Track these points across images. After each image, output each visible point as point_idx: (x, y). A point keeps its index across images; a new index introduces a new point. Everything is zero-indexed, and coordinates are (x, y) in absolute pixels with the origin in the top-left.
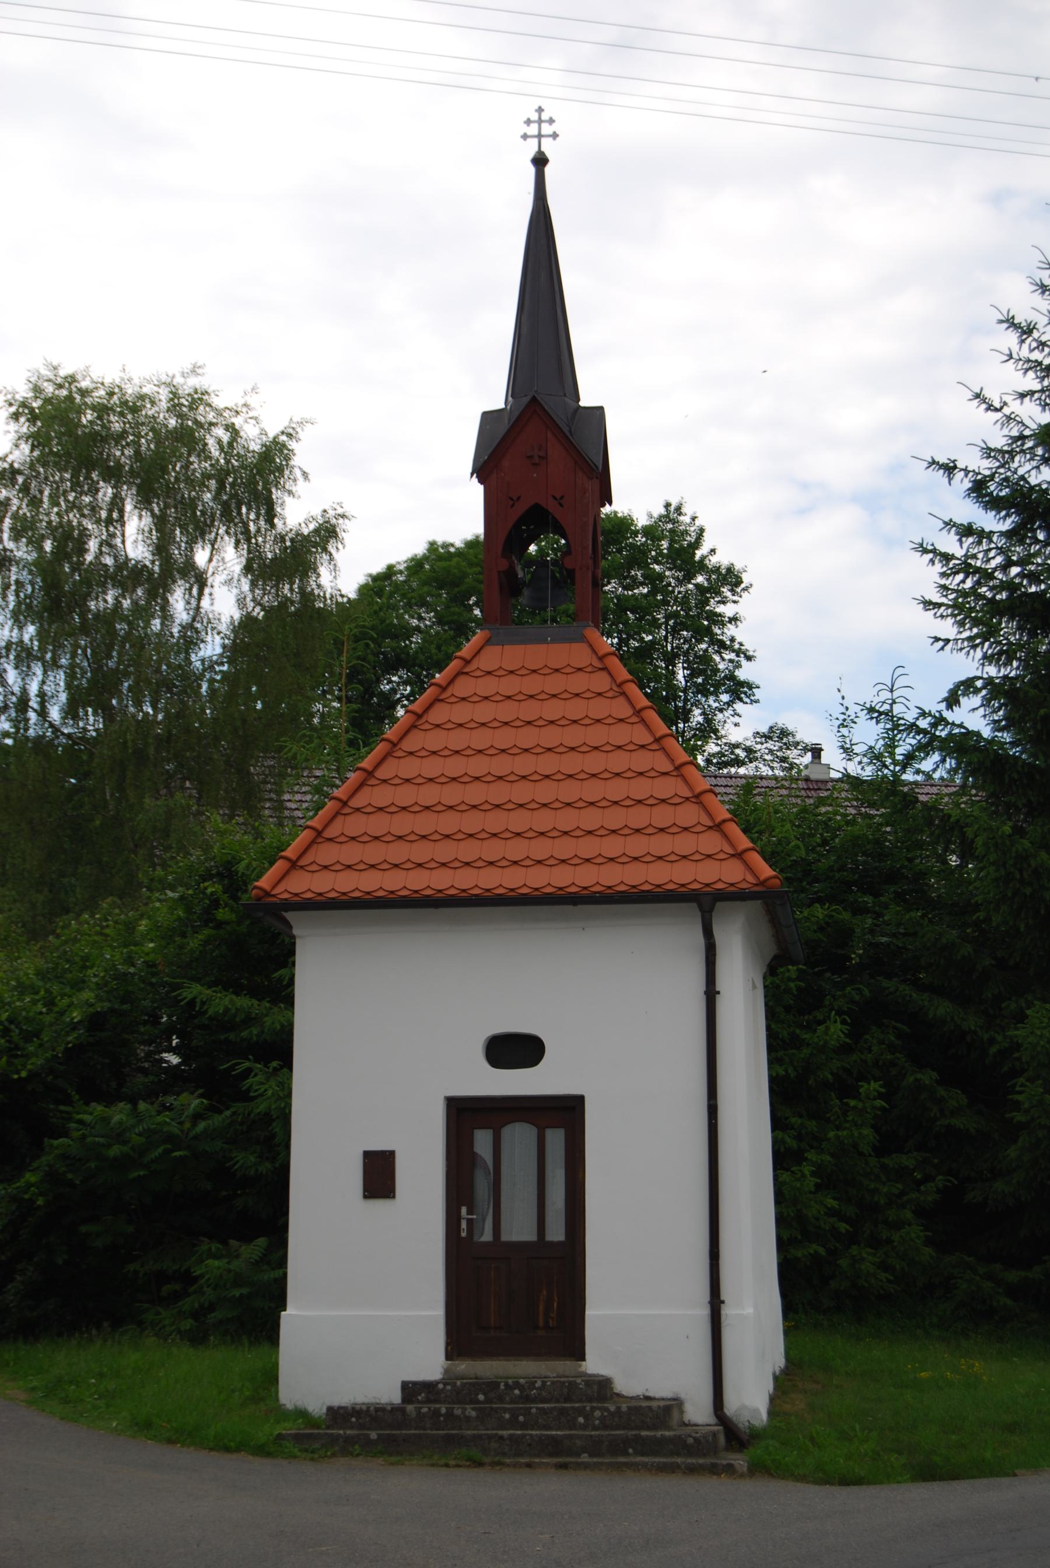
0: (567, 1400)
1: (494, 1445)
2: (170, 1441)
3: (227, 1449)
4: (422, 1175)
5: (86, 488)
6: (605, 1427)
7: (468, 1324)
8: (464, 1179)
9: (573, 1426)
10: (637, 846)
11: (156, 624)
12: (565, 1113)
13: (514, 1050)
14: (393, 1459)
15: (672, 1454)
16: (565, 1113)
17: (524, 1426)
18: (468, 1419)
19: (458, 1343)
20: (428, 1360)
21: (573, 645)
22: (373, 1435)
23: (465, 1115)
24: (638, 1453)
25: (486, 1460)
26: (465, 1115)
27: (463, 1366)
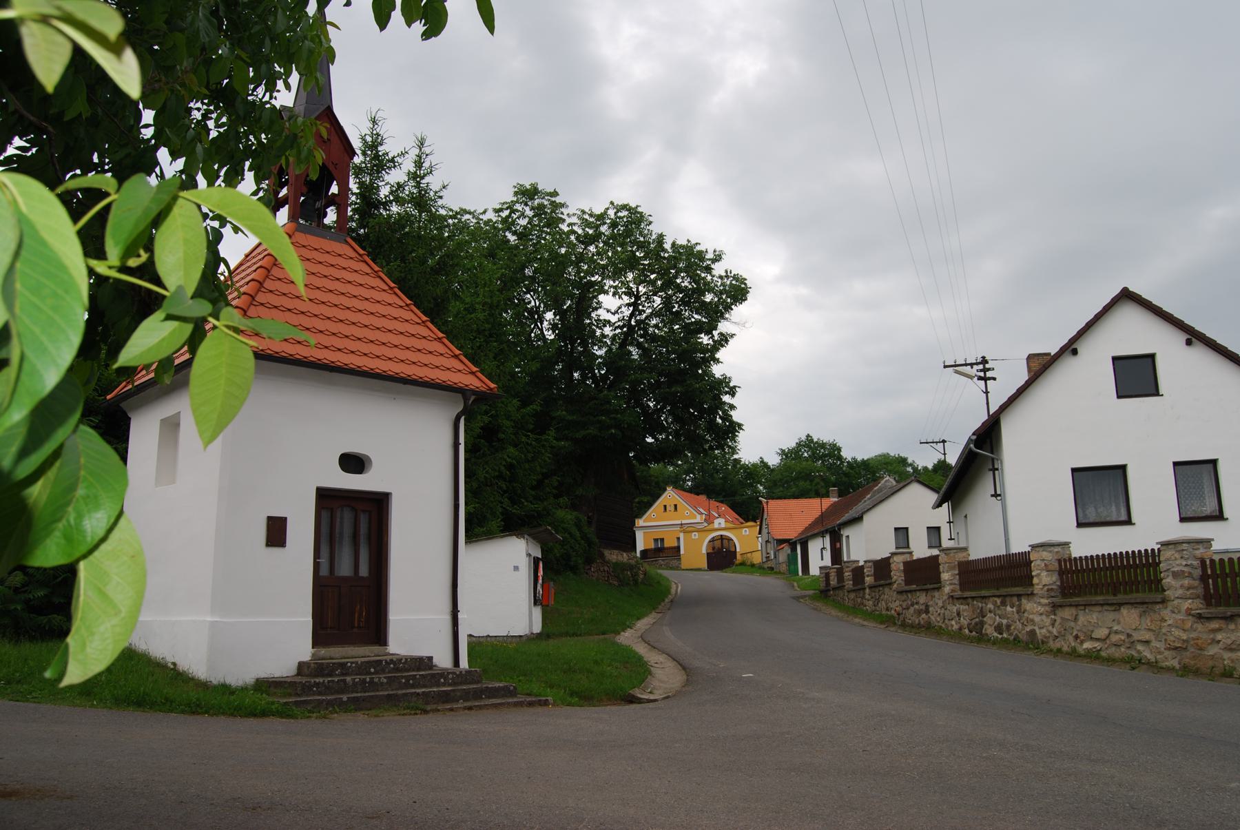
0: (419, 670)
1: (414, 699)
2: (232, 715)
3: (255, 715)
4: (302, 532)
5: (572, 238)
6: (454, 684)
7: (327, 627)
8: (325, 537)
9: (438, 685)
10: (414, 357)
11: (608, 330)
12: (378, 504)
13: (353, 463)
14: (374, 712)
15: (503, 696)
16: (378, 504)
17: (413, 686)
18: (382, 684)
19: (320, 636)
20: (303, 649)
21: (1002, 552)
22: (345, 699)
23: (326, 497)
24: (489, 698)
25: (429, 708)
26: (326, 497)
27: (323, 652)
